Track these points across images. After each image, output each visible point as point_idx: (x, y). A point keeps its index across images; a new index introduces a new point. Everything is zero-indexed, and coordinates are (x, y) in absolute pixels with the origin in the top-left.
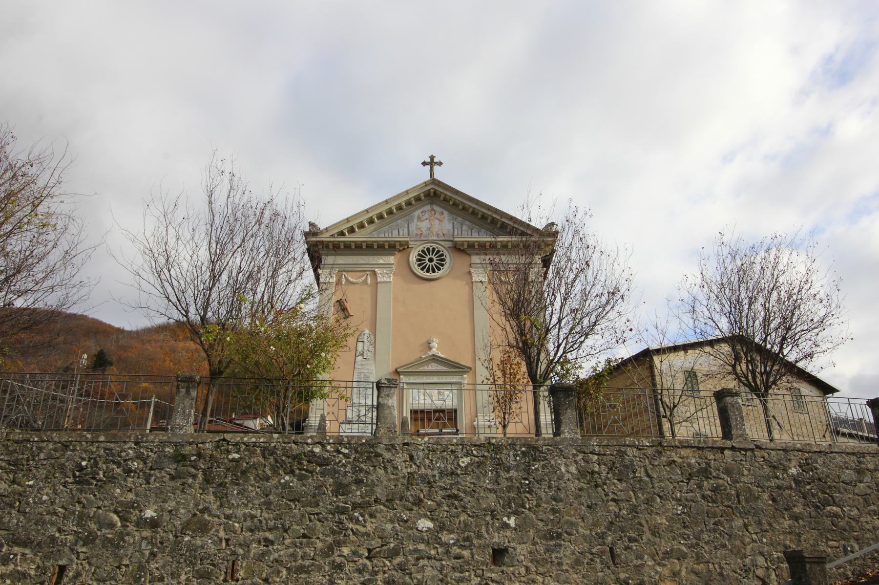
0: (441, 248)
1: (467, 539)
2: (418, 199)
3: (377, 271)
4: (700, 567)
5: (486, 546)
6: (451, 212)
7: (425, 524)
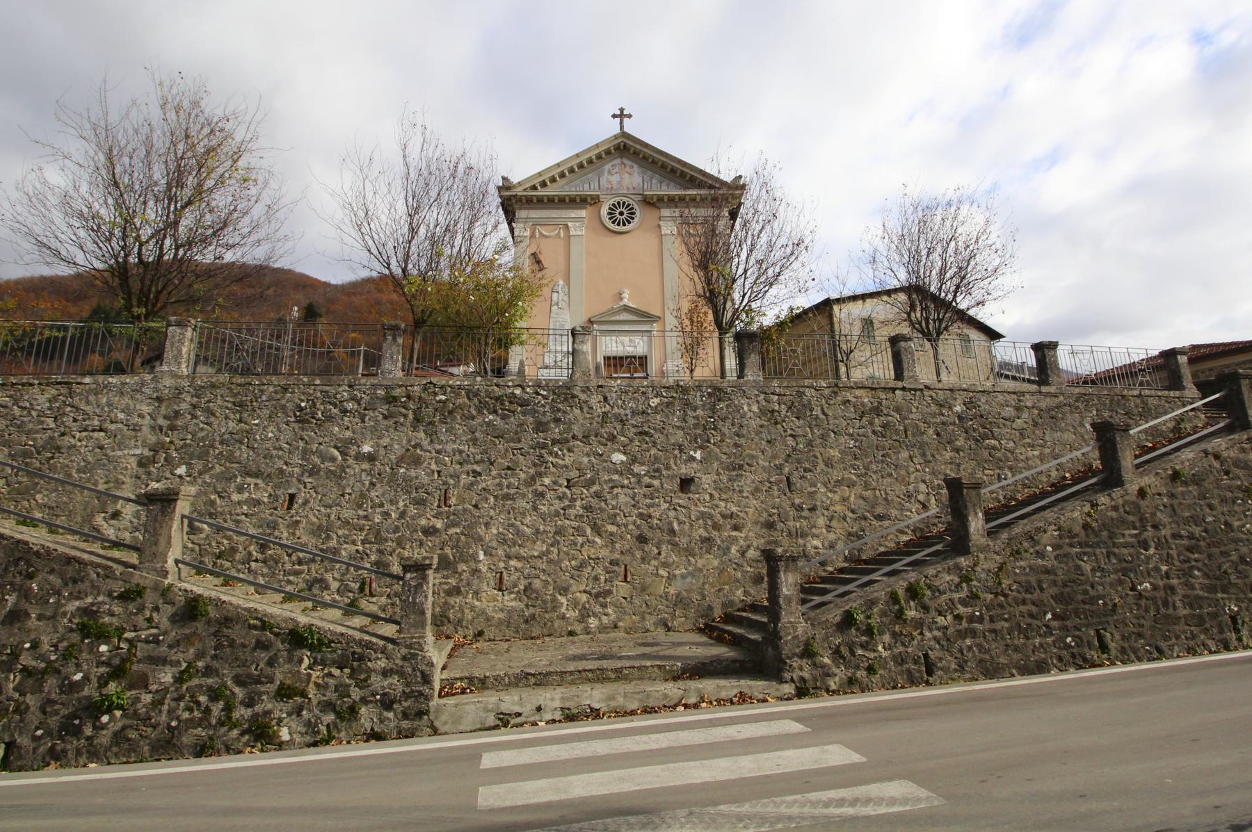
0: (631, 202)
2: (608, 152)
3: (570, 224)
5: (674, 476)
6: (640, 166)
7: (618, 457)
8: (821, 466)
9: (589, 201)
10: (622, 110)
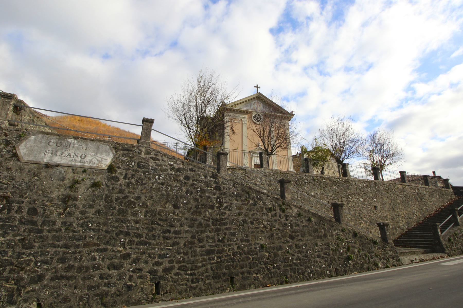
0: (261, 115)
1: (369, 204)
2: (254, 98)
3: (243, 119)
4: (407, 212)
5: (373, 205)
6: (263, 104)
7: (362, 200)
8: (397, 205)
9: (249, 113)
10: (257, 85)
